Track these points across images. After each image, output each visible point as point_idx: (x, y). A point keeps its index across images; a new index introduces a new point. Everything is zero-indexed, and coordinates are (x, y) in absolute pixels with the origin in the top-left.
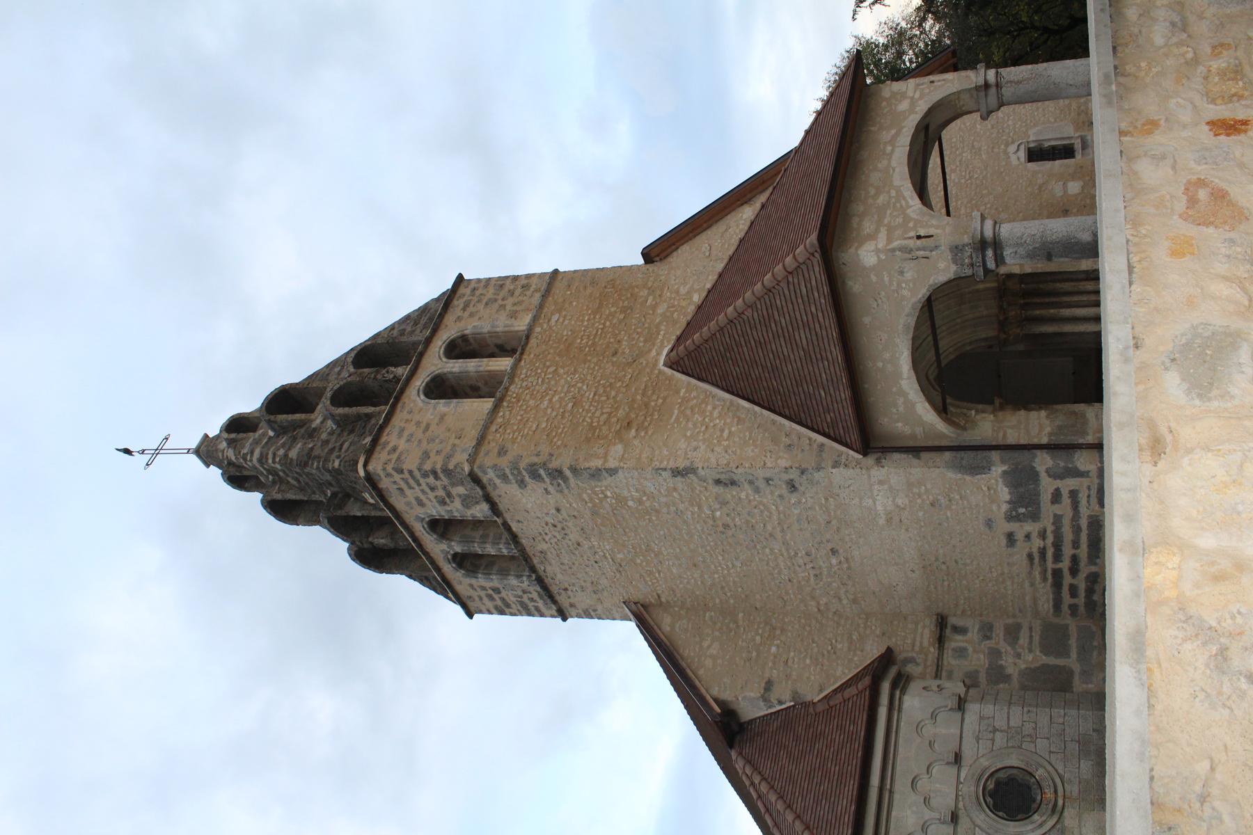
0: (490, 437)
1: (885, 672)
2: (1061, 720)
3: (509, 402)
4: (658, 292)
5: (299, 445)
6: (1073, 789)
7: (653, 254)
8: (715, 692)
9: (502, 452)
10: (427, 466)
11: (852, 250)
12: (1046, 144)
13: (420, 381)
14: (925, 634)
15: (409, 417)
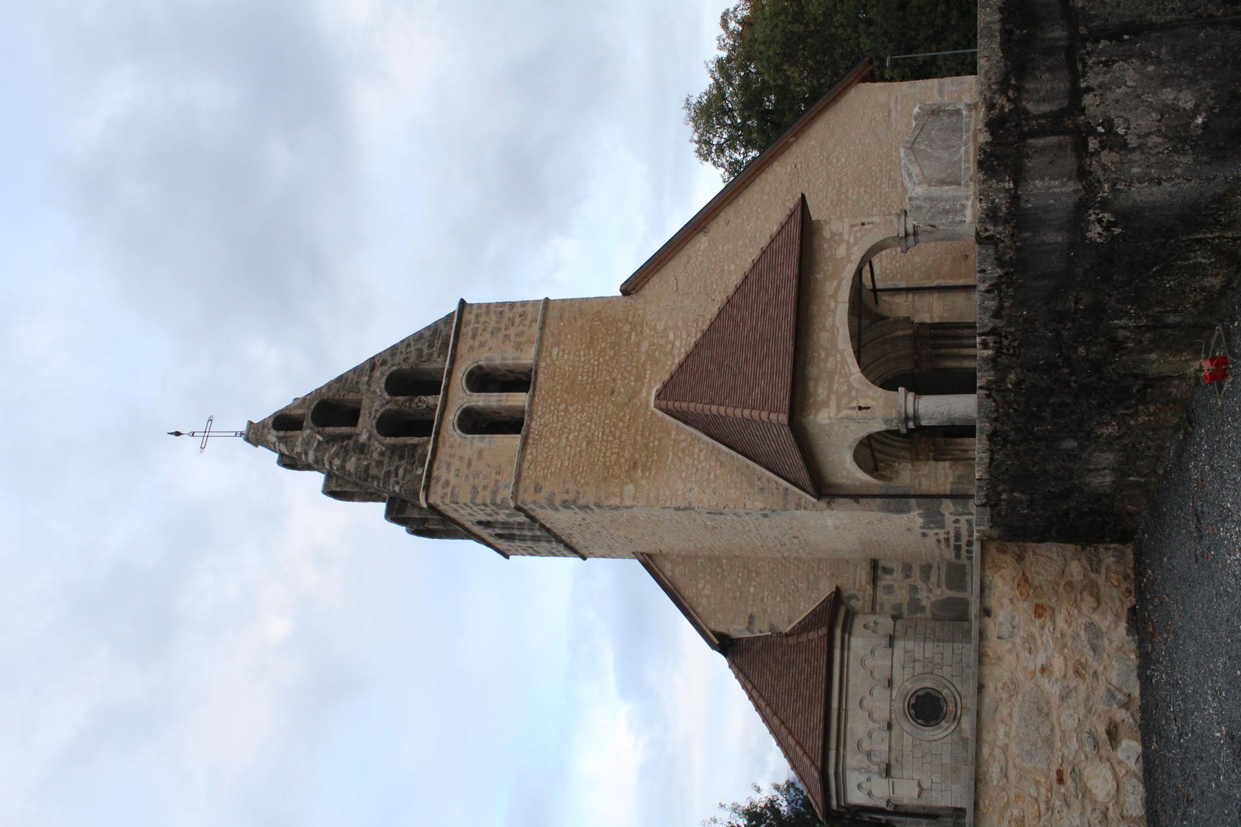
1: (834, 614)
3: (534, 439)
4: (639, 329)
5: (353, 459)
7: (631, 287)
8: (712, 625)
9: (538, 489)
10: (479, 501)
11: (811, 417)
13: (452, 416)
14: (863, 575)
15: (451, 451)
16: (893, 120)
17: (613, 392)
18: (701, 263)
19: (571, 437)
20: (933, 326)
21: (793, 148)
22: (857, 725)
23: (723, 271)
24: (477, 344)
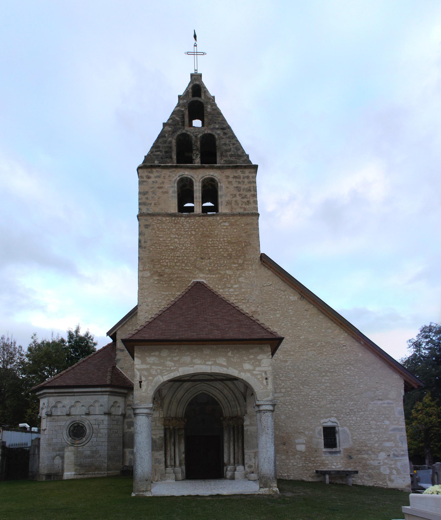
0: (155, 218)
2: (103, 445)
3: (174, 220)
4: (240, 268)
5: (170, 129)
6: (80, 449)
7: (265, 260)
12: (337, 436)
13: (187, 173)
15: (167, 176)
16: (375, 402)
17: (202, 259)
18: (281, 298)
19: (176, 240)
20: (243, 426)
21: (357, 344)
22: (67, 401)
23: (276, 310)
24: (231, 179)
